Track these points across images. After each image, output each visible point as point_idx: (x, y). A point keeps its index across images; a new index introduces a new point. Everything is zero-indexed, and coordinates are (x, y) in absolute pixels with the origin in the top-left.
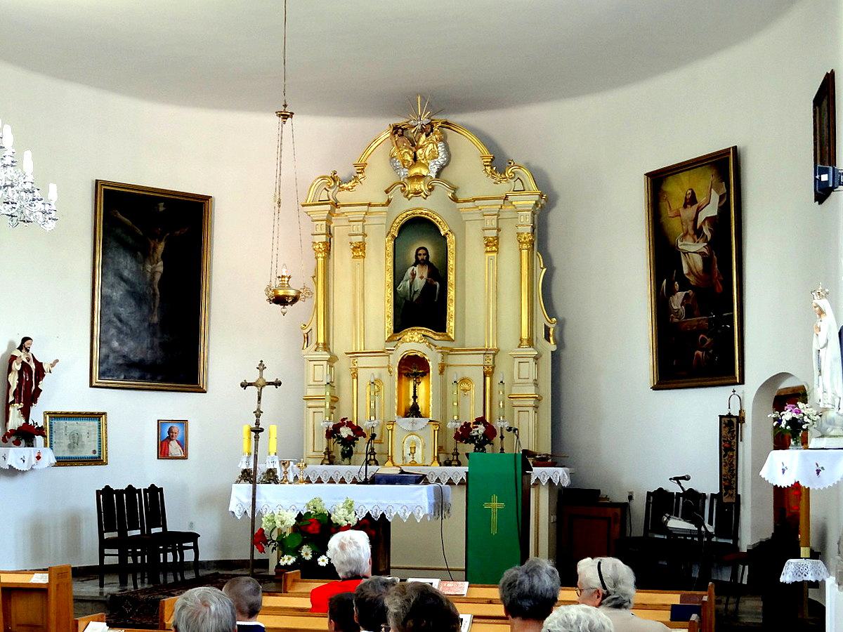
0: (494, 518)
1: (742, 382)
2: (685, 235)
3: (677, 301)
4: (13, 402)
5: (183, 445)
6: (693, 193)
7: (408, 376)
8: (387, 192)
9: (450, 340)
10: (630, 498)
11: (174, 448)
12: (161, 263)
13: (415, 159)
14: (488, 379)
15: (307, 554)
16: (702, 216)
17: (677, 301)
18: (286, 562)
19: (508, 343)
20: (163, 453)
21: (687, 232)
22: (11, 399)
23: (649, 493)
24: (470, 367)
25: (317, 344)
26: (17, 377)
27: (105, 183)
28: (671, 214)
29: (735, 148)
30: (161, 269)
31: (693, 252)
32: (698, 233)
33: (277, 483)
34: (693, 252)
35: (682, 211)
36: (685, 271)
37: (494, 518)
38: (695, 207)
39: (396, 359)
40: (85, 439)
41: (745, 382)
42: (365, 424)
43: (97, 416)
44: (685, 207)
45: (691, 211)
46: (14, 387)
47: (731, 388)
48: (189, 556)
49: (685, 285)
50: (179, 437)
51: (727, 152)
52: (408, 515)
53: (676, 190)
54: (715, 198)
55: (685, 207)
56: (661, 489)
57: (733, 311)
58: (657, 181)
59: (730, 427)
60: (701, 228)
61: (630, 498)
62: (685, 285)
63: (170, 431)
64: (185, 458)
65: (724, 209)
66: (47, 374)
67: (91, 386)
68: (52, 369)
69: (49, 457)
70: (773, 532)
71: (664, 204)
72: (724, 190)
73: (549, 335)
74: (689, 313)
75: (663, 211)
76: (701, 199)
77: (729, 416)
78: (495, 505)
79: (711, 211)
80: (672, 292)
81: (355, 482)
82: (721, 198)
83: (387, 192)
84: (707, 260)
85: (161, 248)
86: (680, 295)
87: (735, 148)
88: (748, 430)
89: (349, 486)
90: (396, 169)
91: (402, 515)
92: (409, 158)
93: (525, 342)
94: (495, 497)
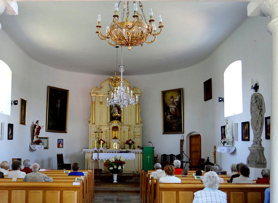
0: (149, 160)
1: (184, 133)
2: (170, 104)
3: (169, 117)
4: (35, 135)
5: (62, 145)
6: (173, 96)
7: (113, 130)
8: (108, 92)
9: (122, 123)
10: (157, 156)
11: (61, 145)
12: (59, 105)
13: (115, 85)
14: (129, 131)
15: (115, 167)
16: (175, 101)
17: (169, 117)
18: (111, 169)
19: (133, 124)
20: (59, 147)
21: (171, 103)
22: (35, 134)
23: (162, 155)
24: (126, 129)
25: (93, 123)
26: (36, 129)
27: (50, 87)
28: (167, 100)
29: (182, 88)
30: (59, 106)
31: (172, 108)
32: (174, 104)
33: (103, 153)
34: (172, 108)
35: (170, 99)
36: (171, 111)
37: (149, 160)
38: (173, 99)
39: (111, 127)
40: (45, 143)
41: (12, 124)
42: (105, 141)
43: (47, 138)
44: (171, 98)
45: (172, 100)
46: (36, 132)
47: (182, 134)
48: (120, 168)
49: (170, 114)
50: (62, 143)
51: (181, 89)
52: (131, 159)
53: (169, 95)
54: (178, 97)
55: (171, 98)
56: (165, 154)
57: (182, 119)
58: (164, 93)
59: (182, 141)
60: (174, 103)
61: (157, 156)
62: (170, 114)
63: (60, 142)
64: (63, 148)
65: (180, 100)
66: (41, 129)
67: (46, 131)
68: (43, 128)
69: (43, 147)
70: (211, 162)
71: (166, 97)
72: (180, 96)
73: (141, 123)
74: (171, 119)
75: (165, 99)
76: (175, 97)
77: (182, 140)
78: (149, 157)
79: (177, 100)
80: (167, 115)
81: (118, 153)
82: (179, 97)
83: (108, 92)
84: (176, 109)
85: (60, 101)
86: (169, 116)
87: (182, 88)
88: (185, 143)
89: (117, 153)
90: (110, 87)
91: (130, 159)
92: (114, 85)
93: (137, 124)
94: (149, 155)
